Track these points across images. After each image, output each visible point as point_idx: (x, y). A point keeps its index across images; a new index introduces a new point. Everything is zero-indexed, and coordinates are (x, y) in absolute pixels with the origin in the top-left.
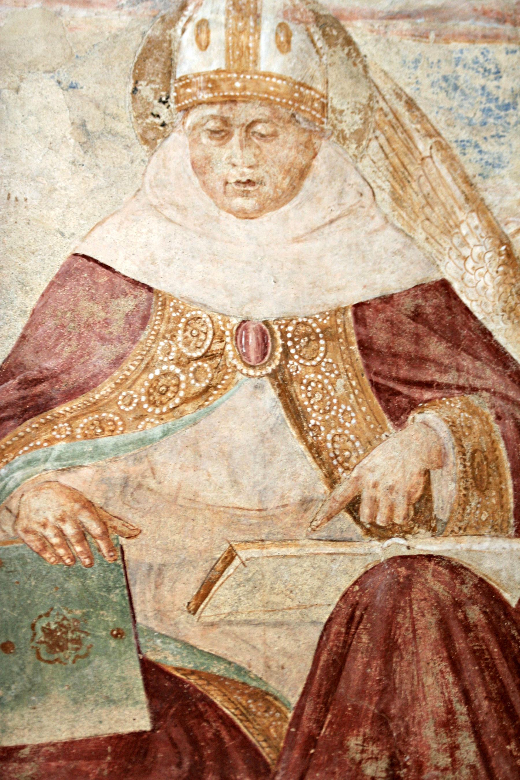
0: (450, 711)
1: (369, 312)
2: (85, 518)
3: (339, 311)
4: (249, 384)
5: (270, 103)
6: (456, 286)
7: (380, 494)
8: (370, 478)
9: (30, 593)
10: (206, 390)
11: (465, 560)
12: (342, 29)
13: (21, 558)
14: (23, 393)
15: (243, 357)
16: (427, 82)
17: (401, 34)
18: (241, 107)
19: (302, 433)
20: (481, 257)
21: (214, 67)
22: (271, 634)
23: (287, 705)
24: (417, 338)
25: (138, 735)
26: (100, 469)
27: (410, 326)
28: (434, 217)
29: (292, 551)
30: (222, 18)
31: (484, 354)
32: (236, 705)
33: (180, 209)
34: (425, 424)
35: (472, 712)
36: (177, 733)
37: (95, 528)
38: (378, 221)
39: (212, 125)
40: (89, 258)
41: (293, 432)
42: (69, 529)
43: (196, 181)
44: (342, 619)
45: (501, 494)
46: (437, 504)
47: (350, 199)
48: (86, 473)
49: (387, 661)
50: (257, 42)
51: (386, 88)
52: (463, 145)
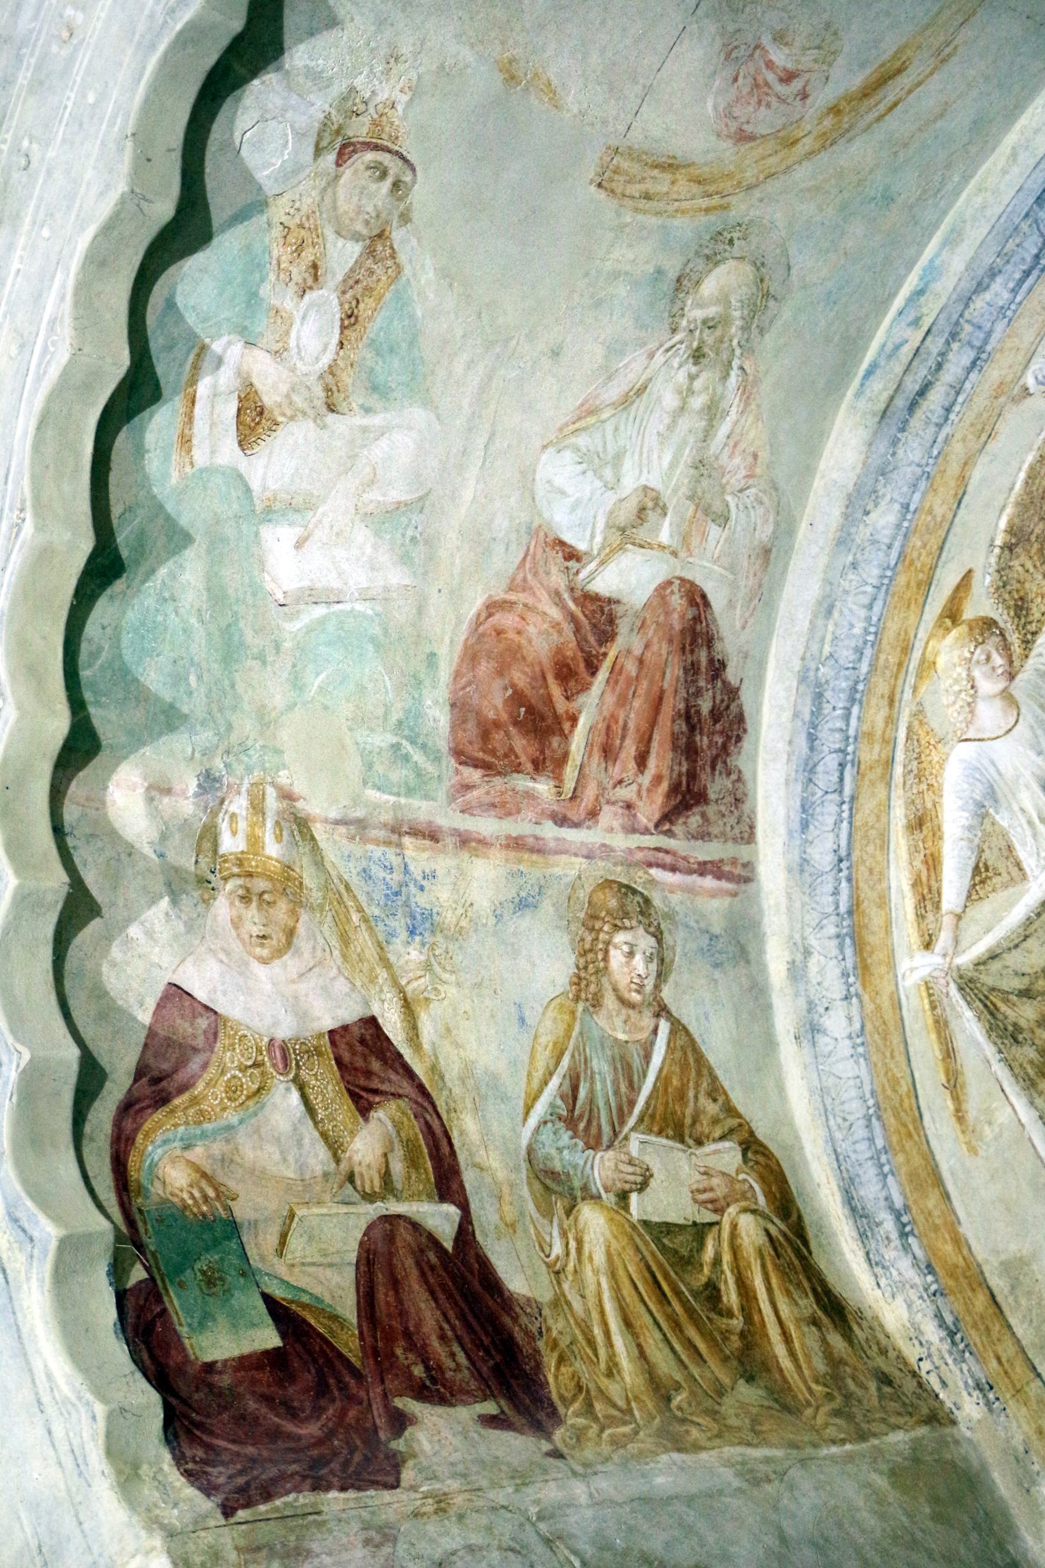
0: (441, 1328)
1: (337, 1037)
2: (204, 1184)
3: (320, 1035)
4: (282, 1087)
5: (271, 879)
6: (380, 1021)
7: (364, 1170)
8: (357, 1158)
9: (185, 1242)
10: (259, 1090)
11: (417, 1218)
12: (309, 829)
13: (172, 1215)
14: (153, 1088)
15: (274, 1066)
16: (354, 871)
17: (340, 835)
18: (255, 880)
19: (316, 1123)
20: (391, 1000)
21: (240, 849)
22: (328, 1272)
23: (351, 1324)
24: (365, 1057)
25: (276, 1350)
26: (207, 1148)
27: (359, 1048)
28: (365, 970)
29: (324, 1211)
30: (244, 813)
31: (401, 1071)
32: (325, 1326)
33: (228, 953)
34: (380, 1120)
35: (453, 1328)
36: (299, 1347)
37: (211, 1193)
38: (335, 971)
39: (241, 892)
40: (179, 987)
41: (310, 1123)
42: (197, 1194)
43: (234, 933)
44: (363, 1262)
45: (427, 1173)
46: (395, 1178)
47: (319, 953)
48: (199, 1150)
49: (397, 1292)
50: (264, 833)
51: (333, 873)
52: (376, 918)
